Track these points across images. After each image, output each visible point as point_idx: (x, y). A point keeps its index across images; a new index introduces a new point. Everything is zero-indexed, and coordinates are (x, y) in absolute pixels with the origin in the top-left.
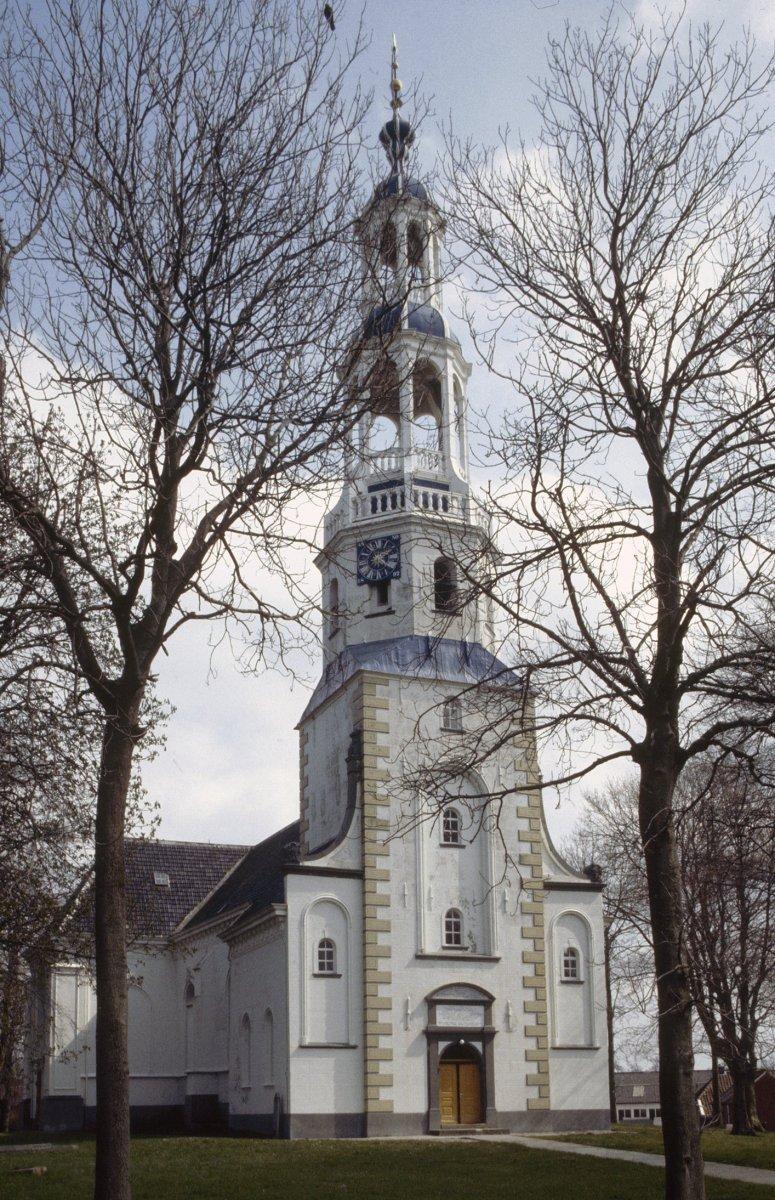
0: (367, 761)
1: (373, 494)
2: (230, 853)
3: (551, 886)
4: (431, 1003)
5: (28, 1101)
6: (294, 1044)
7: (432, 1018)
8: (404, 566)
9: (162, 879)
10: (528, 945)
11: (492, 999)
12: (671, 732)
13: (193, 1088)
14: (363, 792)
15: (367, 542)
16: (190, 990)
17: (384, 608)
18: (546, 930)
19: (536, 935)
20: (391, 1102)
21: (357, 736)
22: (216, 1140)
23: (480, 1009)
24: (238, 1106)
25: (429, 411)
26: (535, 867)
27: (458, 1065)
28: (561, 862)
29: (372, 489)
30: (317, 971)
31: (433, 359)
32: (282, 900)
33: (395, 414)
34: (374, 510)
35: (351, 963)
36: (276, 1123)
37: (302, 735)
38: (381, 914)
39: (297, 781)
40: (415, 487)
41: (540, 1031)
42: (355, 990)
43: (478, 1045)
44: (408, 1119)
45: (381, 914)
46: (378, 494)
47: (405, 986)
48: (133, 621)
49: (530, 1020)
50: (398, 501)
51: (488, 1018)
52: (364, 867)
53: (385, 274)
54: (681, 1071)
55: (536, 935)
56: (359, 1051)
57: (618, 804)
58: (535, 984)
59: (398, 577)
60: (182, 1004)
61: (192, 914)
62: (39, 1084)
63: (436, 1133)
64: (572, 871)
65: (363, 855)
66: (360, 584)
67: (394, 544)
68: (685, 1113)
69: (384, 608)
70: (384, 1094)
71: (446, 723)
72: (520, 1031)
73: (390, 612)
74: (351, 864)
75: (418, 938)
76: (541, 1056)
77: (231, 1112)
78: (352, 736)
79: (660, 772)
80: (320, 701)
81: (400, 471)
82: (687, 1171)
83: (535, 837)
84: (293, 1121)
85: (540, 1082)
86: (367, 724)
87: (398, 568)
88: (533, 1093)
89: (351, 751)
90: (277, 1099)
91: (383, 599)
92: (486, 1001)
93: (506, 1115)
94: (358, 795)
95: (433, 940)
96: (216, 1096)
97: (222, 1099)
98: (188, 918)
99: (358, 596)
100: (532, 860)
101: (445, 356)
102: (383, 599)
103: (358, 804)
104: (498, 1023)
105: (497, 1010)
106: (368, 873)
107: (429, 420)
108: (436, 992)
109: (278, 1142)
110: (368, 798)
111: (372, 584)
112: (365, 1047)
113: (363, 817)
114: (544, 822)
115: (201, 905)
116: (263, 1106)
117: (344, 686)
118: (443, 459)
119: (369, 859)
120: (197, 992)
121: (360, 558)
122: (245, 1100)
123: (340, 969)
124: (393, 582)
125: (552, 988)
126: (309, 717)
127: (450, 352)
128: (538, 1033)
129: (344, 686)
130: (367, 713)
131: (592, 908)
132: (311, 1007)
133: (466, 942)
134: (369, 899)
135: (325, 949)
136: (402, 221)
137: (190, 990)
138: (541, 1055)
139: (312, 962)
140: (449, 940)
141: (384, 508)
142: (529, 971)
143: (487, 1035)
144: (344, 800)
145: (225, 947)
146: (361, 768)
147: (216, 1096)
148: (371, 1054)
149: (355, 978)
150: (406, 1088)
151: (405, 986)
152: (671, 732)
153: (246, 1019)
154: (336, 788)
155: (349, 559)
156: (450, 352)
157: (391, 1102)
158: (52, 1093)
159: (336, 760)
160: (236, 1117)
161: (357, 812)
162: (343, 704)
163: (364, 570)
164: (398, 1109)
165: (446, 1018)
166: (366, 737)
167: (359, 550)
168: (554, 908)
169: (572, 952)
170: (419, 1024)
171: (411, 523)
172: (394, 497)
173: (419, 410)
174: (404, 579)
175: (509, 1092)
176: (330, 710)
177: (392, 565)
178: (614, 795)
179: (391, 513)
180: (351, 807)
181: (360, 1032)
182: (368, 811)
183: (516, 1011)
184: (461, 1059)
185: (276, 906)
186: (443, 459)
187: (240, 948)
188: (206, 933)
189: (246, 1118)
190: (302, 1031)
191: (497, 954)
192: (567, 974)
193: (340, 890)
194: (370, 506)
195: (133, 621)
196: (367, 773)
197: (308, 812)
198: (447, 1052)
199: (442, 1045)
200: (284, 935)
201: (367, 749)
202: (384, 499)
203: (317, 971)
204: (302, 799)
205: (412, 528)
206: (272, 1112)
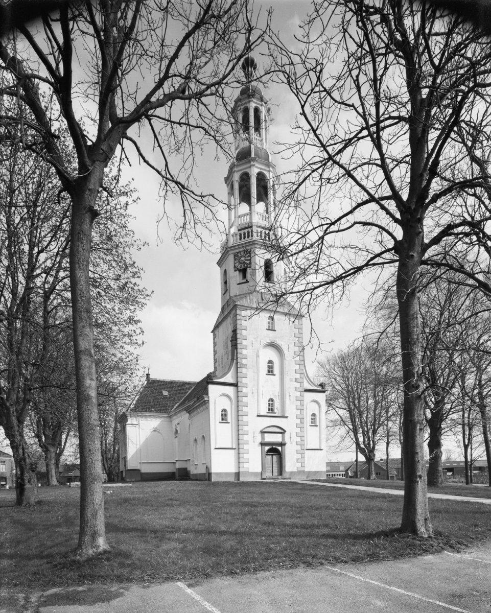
0: (239, 341)
1: (240, 232)
2: (190, 384)
3: (307, 390)
4: (263, 432)
5: (122, 471)
6: (213, 447)
7: (263, 438)
8: (253, 263)
9: (165, 393)
10: (298, 412)
11: (285, 431)
12: (420, 230)
13: (178, 466)
14: (237, 353)
15: (238, 253)
16: (176, 431)
17: (245, 281)
18: (305, 407)
19: (301, 408)
20: (248, 468)
21: (235, 331)
22: (184, 482)
23: (281, 435)
24: (193, 471)
25: (263, 200)
26: (301, 383)
27: (272, 455)
28: (310, 381)
29: (239, 230)
30: (221, 421)
31: (265, 172)
32: (207, 394)
33: (249, 202)
34: (240, 239)
35: (235, 417)
36: (207, 476)
37: (214, 335)
38: (245, 419)
39: (213, 344)
40: (257, 229)
41: (302, 443)
42: (234, 426)
43: (280, 448)
44: (255, 474)
45: (245, 399)
46: (242, 232)
47: (254, 425)
48: (89, 143)
49: (299, 439)
50: (250, 234)
51: (283, 438)
52: (238, 382)
53: (244, 208)
54: (418, 428)
55: (301, 408)
56: (236, 450)
57: (329, 365)
58: (301, 426)
59: (250, 267)
60: (174, 435)
61: (177, 405)
62: (125, 466)
63: (265, 479)
64: (315, 385)
65: (237, 378)
66: (235, 271)
67: (248, 253)
68: (418, 450)
69: (245, 281)
70: (246, 465)
71: (269, 327)
72: (294, 443)
73: (247, 282)
74: (232, 381)
75: (258, 411)
76: (303, 449)
77: (191, 473)
78: (233, 331)
79: (412, 256)
80: (220, 320)
81: (251, 222)
82: (419, 483)
83: (301, 372)
84: (213, 475)
85: (301, 461)
86: (238, 327)
87: (250, 263)
88: (299, 465)
89: (232, 337)
90: (207, 467)
91: (245, 276)
92: (283, 432)
93: (291, 473)
94: (235, 354)
95: (264, 410)
96: (186, 468)
97: (188, 469)
98: (175, 407)
99: (235, 277)
100: (301, 380)
101: (269, 171)
102: (245, 276)
103: (235, 358)
104: (287, 440)
105: (286, 435)
106: (239, 384)
107: (262, 205)
108: (264, 429)
109: (207, 482)
110: (239, 356)
111: (240, 270)
112: (239, 449)
113: (237, 363)
114: (305, 366)
115: (180, 402)
116: (201, 470)
117: (229, 313)
118: (268, 218)
119: (239, 379)
120: (179, 432)
121: (235, 259)
122: (196, 469)
123: (229, 420)
124: (248, 269)
125: (307, 428)
126: (217, 327)
127: (271, 169)
128: (301, 444)
129: (229, 313)
130: (238, 322)
131: (321, 397)
132: (221, 434)
133: (276, 411)
134: (240, 394)
135: (223, 413)
136: (252, 105)
137: (176, 431)
138: (302, 452)
139: (219, 418)
140: (269, 410)
141: (244, 238)
142: (298, 421)
143: (282, 444)
144: (230, 357)
145: (188, 415)
146: (236, 344)
147: (186, 468)
148: (241, 451)
149: (234, 421)
150: (254, 464)
151: (254, 425)
152: (420, 230)
153: (196, 440)
154: (227, 353)
155: (230, 262)
156: (271, 169)
157: (248, 468)
158: (129, 468)
159: (227, 342)
160: (193, 475)
161: (235, 361)
162: (229, 320)
163: (237, 265)
164: (251, 471)
165: (269, 438)
166: (238, 331)
167: (235, 256)
168: (309, 396)
169: (314, 415)
170: (259, 439)
171: (255, 244)
172: (248, 233)
173: (259, 199)
174: (253, 267)
175: (290, 465)
176: (224, 325)
177: (248, 262)
178: (328, 361)
179: (247, 240)
180: (233, 359)
181: (237, 443)
182: (239, 360)
183: (294, 435)
184: (275, 451)
185: (205, 396)
186: (268, 218)
187: (192, 415)
188: (181, 411)
189: (196, 475)
190: (216, 443)
191: (286, 415)
192: (312, 423)
193: (230, 390)
194: (238, 237)
195: (89, 143)
196: (239, 346)
197: (217, 364)
198: (269, 451)
199: (267, 448)
200: (208, 408)
201: (239, 336)
202: (245, 234)
203: (221, 421)
204: (214, 360)
205: (256, 246)
206: (205, 472)
